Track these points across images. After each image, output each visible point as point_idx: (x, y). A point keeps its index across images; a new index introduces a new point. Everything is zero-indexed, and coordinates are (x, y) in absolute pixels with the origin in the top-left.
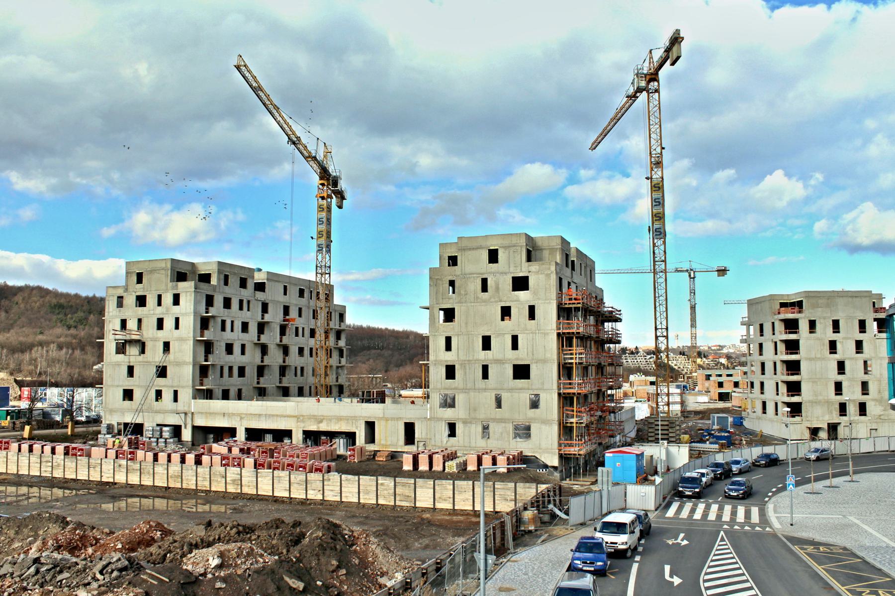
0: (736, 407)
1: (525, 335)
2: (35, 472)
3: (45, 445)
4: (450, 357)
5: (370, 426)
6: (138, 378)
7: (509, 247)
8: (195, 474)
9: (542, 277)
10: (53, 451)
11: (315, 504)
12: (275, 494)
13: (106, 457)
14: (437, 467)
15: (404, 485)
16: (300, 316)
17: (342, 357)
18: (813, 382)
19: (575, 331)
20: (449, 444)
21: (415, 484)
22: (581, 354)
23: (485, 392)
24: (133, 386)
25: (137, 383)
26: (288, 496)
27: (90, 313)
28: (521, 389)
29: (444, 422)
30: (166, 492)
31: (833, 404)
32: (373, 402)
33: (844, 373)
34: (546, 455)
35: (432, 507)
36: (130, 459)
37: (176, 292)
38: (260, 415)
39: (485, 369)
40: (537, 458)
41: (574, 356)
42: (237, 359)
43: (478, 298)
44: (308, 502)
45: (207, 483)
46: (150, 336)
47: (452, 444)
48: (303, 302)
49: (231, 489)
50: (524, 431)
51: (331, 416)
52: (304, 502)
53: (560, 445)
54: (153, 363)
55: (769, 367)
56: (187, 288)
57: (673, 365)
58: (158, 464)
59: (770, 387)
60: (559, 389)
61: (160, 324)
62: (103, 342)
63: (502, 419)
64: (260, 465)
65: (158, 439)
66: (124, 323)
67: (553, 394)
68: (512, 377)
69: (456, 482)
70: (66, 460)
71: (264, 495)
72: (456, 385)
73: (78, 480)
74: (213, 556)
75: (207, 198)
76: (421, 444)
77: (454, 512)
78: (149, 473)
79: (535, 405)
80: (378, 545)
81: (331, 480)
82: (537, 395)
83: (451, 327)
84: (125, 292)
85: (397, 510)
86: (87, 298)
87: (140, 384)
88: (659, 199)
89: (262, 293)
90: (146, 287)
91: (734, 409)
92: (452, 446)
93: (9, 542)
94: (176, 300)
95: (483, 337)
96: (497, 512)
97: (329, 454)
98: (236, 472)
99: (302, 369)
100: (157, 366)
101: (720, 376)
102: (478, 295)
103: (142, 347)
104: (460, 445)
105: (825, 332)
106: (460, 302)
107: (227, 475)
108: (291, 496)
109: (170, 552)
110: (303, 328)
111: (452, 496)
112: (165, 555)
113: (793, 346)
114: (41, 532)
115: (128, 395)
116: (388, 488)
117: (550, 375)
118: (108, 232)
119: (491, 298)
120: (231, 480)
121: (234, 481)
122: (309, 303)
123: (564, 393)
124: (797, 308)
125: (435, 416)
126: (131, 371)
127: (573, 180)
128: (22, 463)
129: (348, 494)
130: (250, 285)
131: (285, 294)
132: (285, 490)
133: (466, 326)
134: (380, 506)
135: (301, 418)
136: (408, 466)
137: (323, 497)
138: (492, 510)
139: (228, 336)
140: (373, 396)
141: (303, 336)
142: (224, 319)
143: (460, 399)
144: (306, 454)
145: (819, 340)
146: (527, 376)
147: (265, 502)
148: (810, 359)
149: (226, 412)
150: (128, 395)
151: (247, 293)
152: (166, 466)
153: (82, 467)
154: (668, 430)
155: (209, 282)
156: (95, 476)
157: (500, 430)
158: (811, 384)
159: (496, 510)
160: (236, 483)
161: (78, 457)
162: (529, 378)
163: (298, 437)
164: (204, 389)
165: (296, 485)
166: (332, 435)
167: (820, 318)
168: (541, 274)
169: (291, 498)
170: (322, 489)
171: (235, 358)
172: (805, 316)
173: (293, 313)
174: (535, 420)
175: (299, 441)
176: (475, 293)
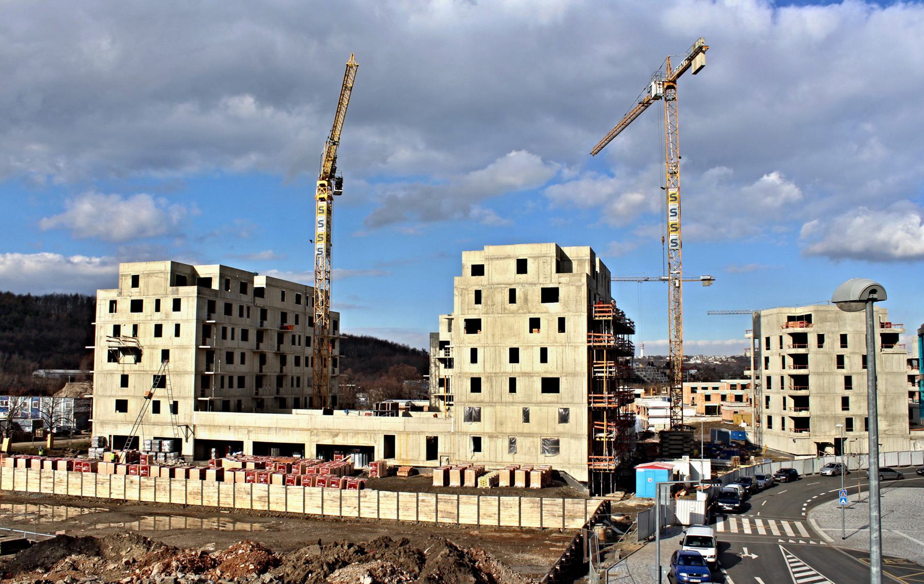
0: (727, 421)
1: (554, 348)
2: (33, 488)
3: (19, 458)
4: (476, 370)
5: (390, 441)
6: (133, 389)
7: (538, 257)
8: (217, 491)
9: (573, 289)
10: (55, 467)
11: (350, 521)
12: (306, 512)
13: (115, 472)
14: (469, 482)
15: (446, 501)
16: (297, 323)
17: (336, 367)
18: (821, 397)
19: (606, 344)
20: (474, 459)
21: (458, 500)
22: (610, 367)
23: (512, 405)
24: (128, 396)
25: (132, 394)
26: (321, 513)
27: (26, 314)
28: (550, 403)
29: (468, 437)
30: (185, 510)
31: (840, 419)
32: (388, 416)
33: (851, 388)
34: (575, 470)
35: (476, 523)
36: (143, 475)
37: (176, 297)
38: (269, 428)
39: (513, 382)
40: (566, 473)
41: (605, 370)
42: (237, 368)
43: (505, 309)
44: (343, 520)
45: (231, 501)
46: (148, 343)
47: (479, 459)
48: (299, 308)
49: (258, 506)
50: (553, 446)
51: (348, 430)
52: (338, 520)
53: (590, 460)
54: (150, 372)
55: (776, 381)
56: (189, 294)
57: (642, 376)
58: (175, 481)
59: (776, 400)
60: (589, 403)
61: (158, 331)
62: (94, 349)
63: (530, 433)
64: (289, 481)
65: (156, 453)
66: (117, 330)
67: (583, 409)
68: (541, 391)
69: (501, 498)
70: (70, 476)
71: (294, 513)
72: (482, 398)
73: (83, 497)
74: (363, 575)
75: (156, 190)
76: (444, 459)
77: (499, 529)
78: (165, 490)
79: (564, 418)
80: (498, 561)
81: (368, 497)
82: (566, 410)
83: (478, 338)
84: (118, 296)
85: (439, 527)
86: (20, 297)
87: (134, 395)
88: (675, 209)
89: (261, 299)
90: (142, 291)
91: (725, 424)
92: (477, 461)
93: (103, 563)
94: (177, 305)
95: (510, 349)
96: (544, 528)
97: (348, 468)
98: (263, 489)
99: (298, 379)
100: (155, 376)
101: (706, 388)
102: (506, 306)
103: (137, 353)
104: (485, 460)
105: (833, 345)
106: (487, 313)
107: (253, 491)
108: (324, 514)
109: (311, 572)
110: (300, 336)
111: (497, 513)
112: (307, 575)
113: (801, 361)
114: (123, 553)
115: (122, 406)
116: (429, 504)
117: (580, 389)
118: (46, 223)
119: (519, 309)
120: (258, 497)
121: (260, 498)
122: (305, 309)
123: (594, 408)
124: (805, 322)
125: (460, 430)
126: (125, 381)
127: (557, 180)
128: (18, 478)
129: (386, 511)
130: (250, 291)
131: (283, 300)
132: (318, 507)
133: (493, 338)
134: (420, 523)
135: (315, 432)
136: (438, 482)
137: (359, 514)
138: (540, 526)
139: (229, 344)
140: (388, 409)
141: (299, 345)
142: (225, 326)
143: (486, 413)
144: (327, 469)
145: (828, 354)
146: (556, 390)
147: (296, 520)
148: (818, 374)
149: (232, 425)
150: (122, 406)
151: (247, 299)
152: (185, 483)
153: (88, 483)
154: (682, 445)
155: (210, 286)
156: (103, 493)
157: (528, 445)
158: (818, 399)
159: (543, 526)
160: (263, 499)
161: (84, 473)
162: (558, 392)
163: (310, 452)
164: (207, 401)
165: (329, 502)
166: (346, 450)
167: (828, 333)
168: (572, 285)
169: (324, 516)
170: (358, 506)
171: (235, 368)
172: (814, 330)
173: (291, 321)
174: (563, 434)
175: (312, 455)
176: (503, 304)
